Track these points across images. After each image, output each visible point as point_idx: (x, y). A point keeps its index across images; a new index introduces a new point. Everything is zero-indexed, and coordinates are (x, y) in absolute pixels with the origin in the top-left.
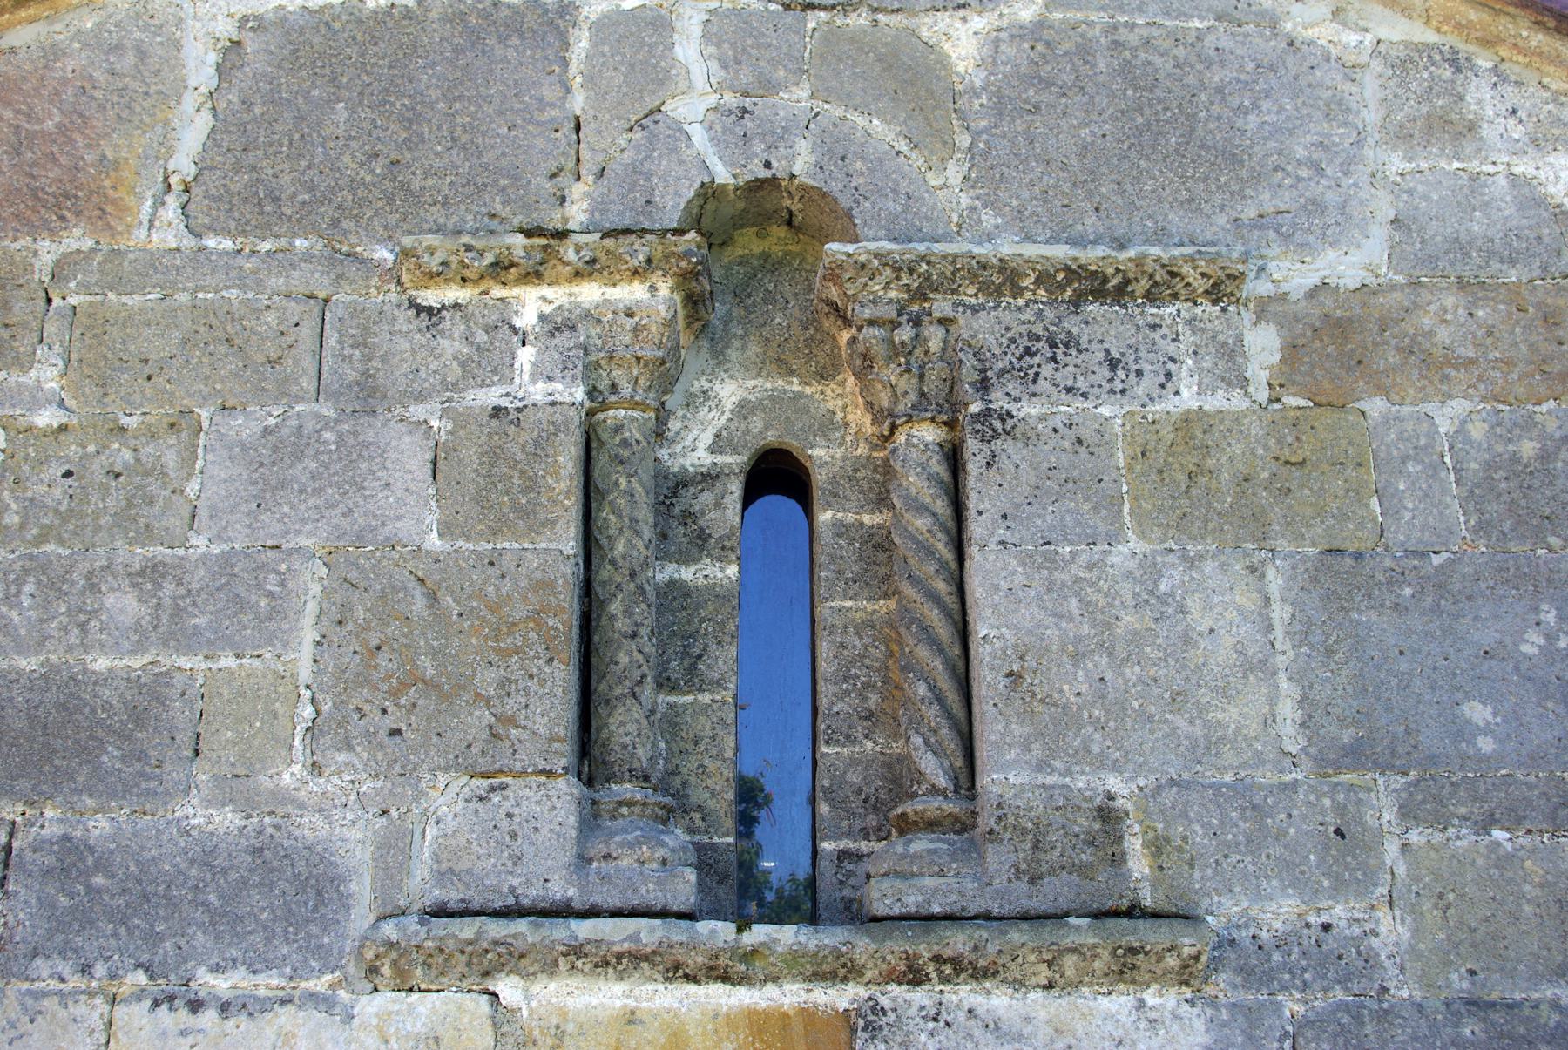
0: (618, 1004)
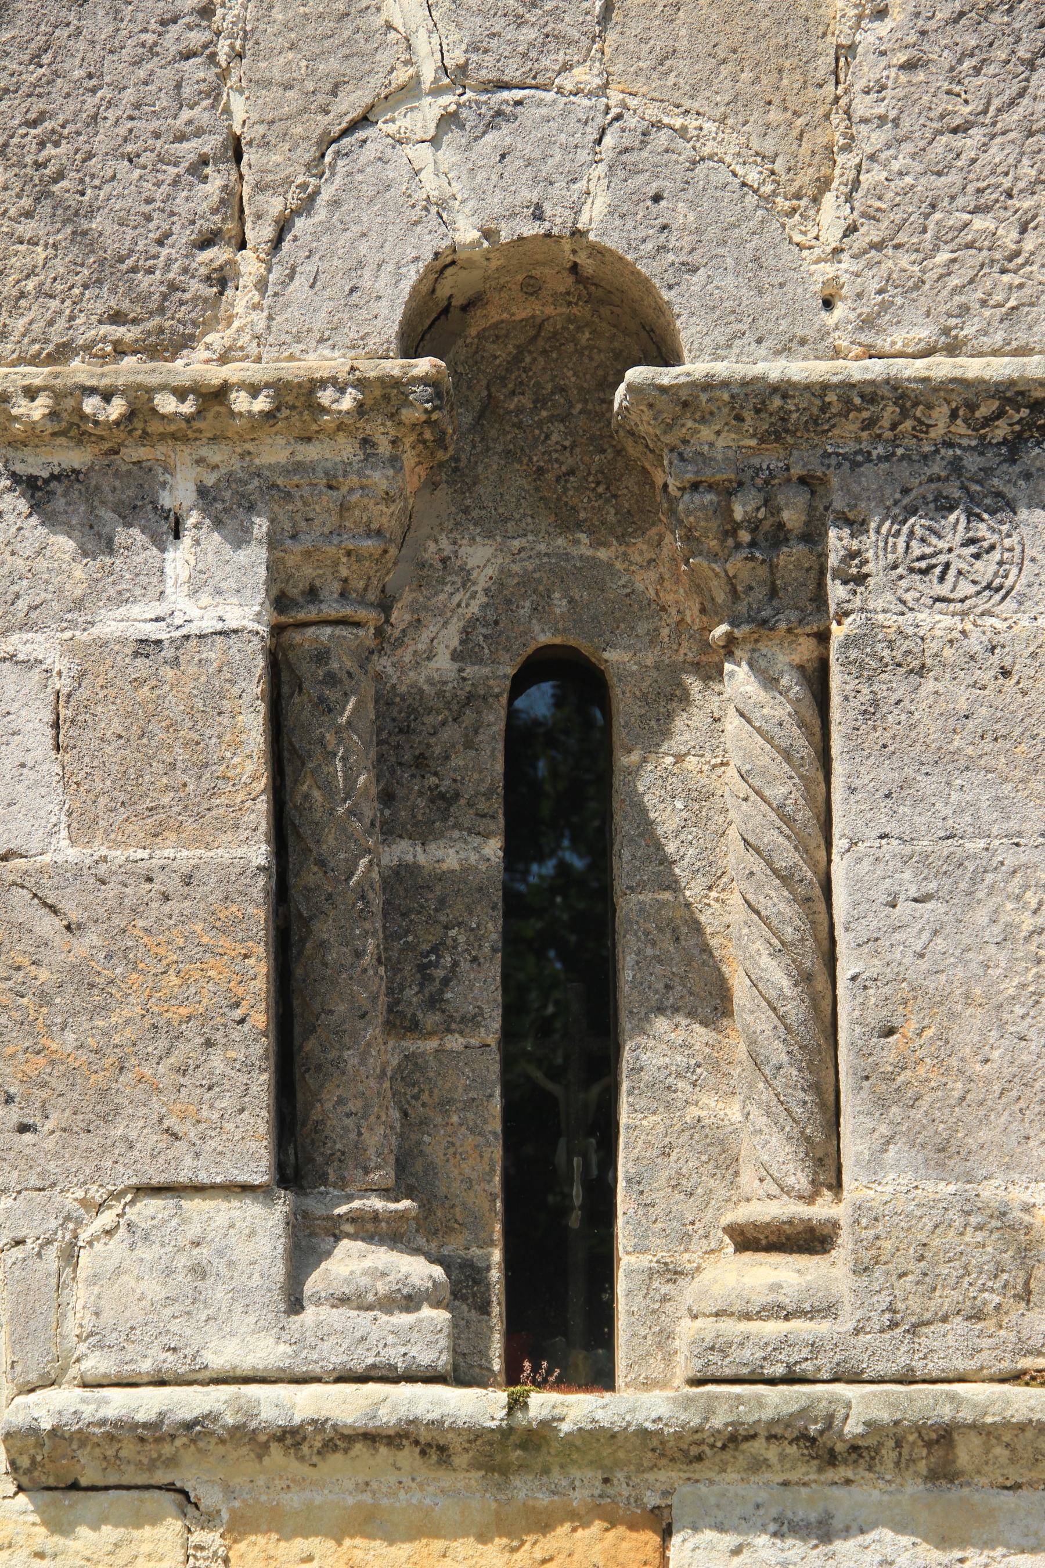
0: (350, 1501)
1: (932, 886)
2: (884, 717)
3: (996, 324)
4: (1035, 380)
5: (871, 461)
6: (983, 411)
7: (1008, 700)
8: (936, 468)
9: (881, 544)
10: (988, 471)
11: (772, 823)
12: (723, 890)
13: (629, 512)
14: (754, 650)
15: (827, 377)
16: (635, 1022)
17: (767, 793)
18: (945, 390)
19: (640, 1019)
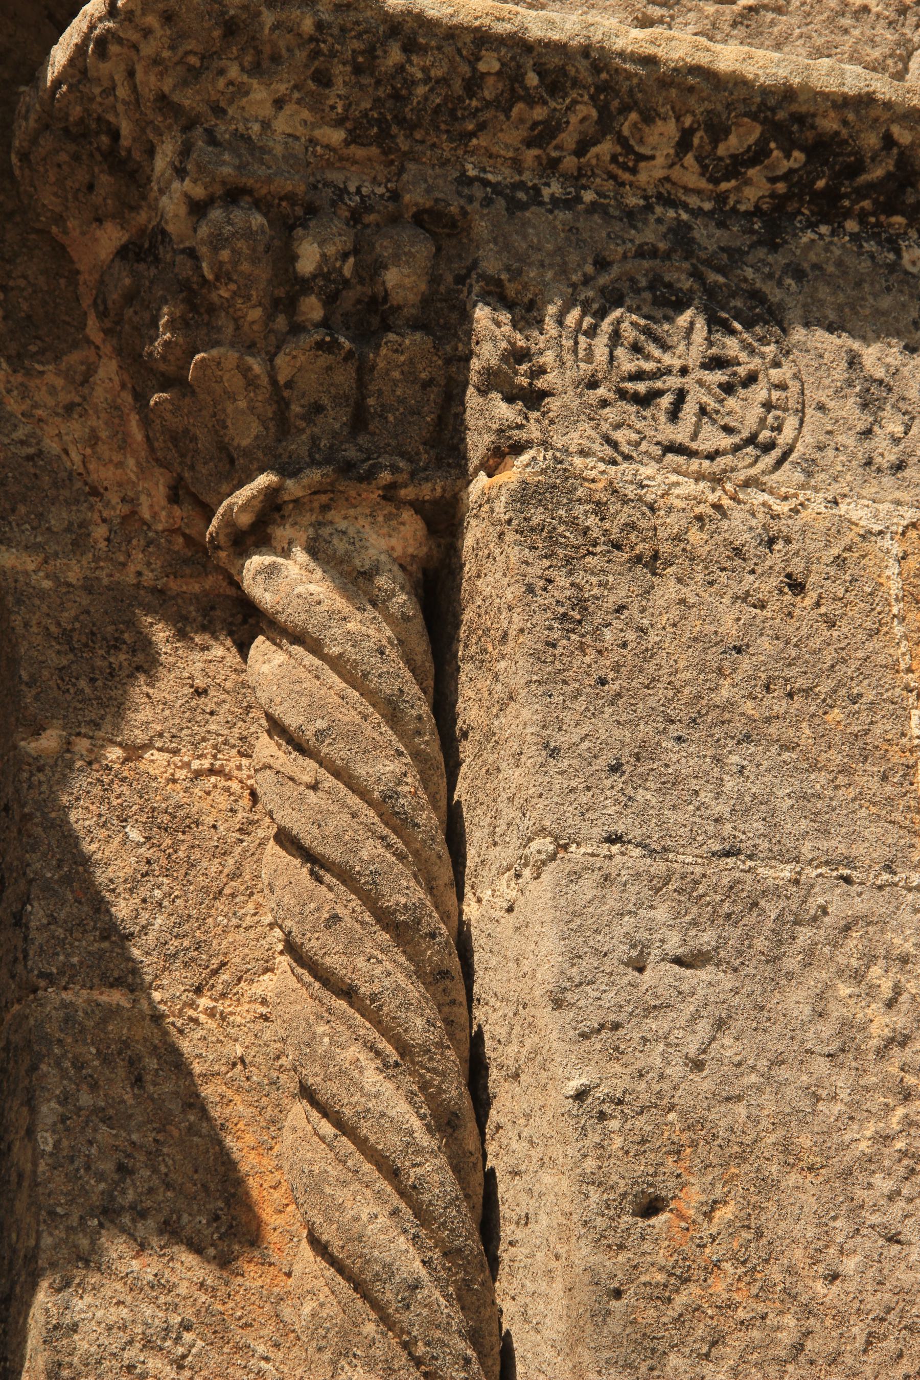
1: (707, 938)
2: (596, 632)
3: (726, 28)
4: (826, 96)
5: (541, 204)
6: (733, 144)
7: (805, 631)
8: (649, 235)
9: (568, 343)
10: (735, 256)
11: (370, 828)
12: (223, 995)
13: (29, 317)
14: (319, 524)
15: (487, 21)
16: (60, 1233)
17: (361, 770)
18: (679, 86)
19: (70, 1229)
